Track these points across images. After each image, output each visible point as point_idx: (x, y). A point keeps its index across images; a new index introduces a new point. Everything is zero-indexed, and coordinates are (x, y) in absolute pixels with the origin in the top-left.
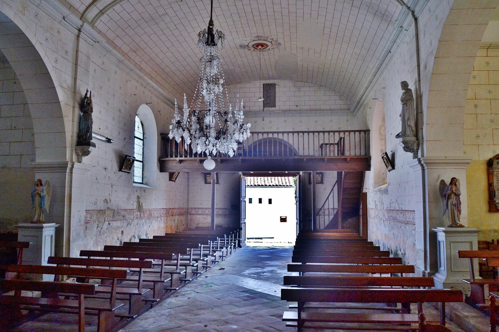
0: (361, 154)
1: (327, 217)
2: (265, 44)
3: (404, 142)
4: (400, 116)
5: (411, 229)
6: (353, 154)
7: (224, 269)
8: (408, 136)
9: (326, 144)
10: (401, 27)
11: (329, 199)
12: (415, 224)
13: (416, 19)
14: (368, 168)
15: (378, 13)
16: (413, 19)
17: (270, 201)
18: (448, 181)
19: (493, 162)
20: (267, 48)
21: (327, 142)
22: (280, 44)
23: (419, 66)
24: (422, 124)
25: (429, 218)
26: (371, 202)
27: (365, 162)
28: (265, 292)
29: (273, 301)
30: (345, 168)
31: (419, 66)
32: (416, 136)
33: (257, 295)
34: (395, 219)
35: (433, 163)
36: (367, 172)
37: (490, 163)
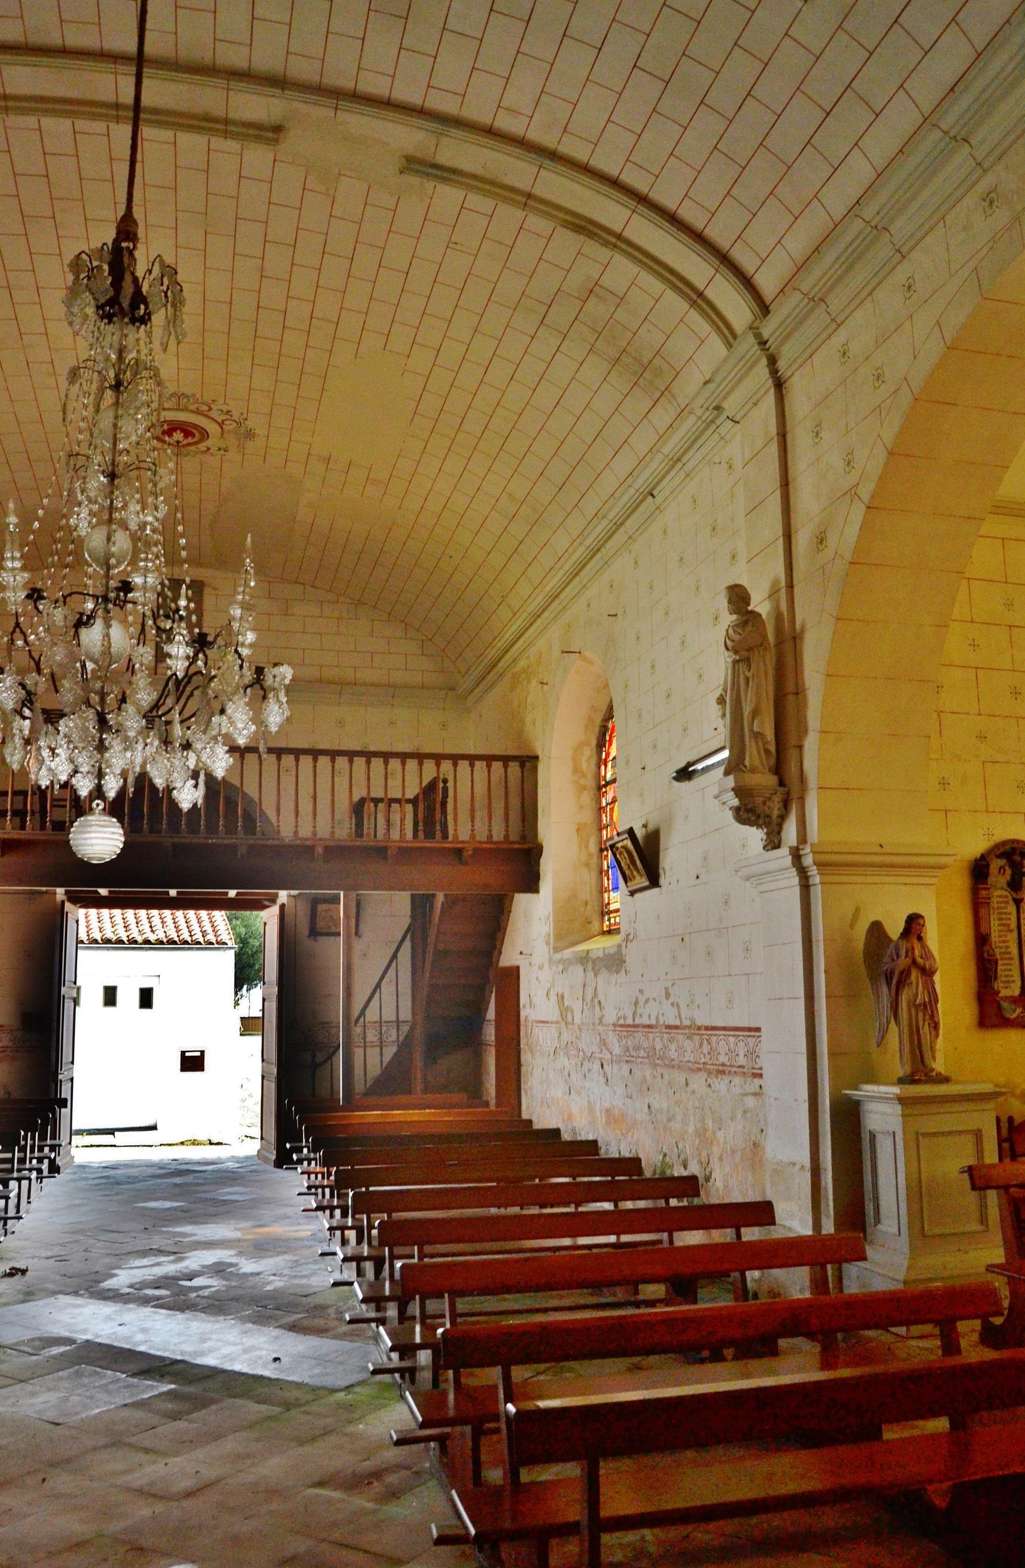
0: (490, 836)
1: (373, 1054)
2: (196, 426)
3: (738, 791)
4: (721, 701)
5: (737, 1091)
6: (481, 835)
7: (24, 1272)
8: (753, 770)
9: (376, 801)
10: (718, 408)
11: (376, 990)
12: (761, 1076)
13: (779, 385)
14: (531, 883)
15: (625, 359)
16: (770, 382)
17: (146, 998)
18: (895, 929)
19: (988, 866)
20: (202, 446)
21: (377, 792)
22: (250, 435)
23: (788, 537)
24: (803, 731)
25: (832, 1054)
26: (539, 999)
27: (523, 865)
28: (237, 1367)
29: (289, 1406)
30: (444, 883)
31: (788, 537)
32: (778, 769)
33: (209, 1384)
34: (656, 1059)
35: (858, 865)
36: (521, 901)
37: (979, 871)
